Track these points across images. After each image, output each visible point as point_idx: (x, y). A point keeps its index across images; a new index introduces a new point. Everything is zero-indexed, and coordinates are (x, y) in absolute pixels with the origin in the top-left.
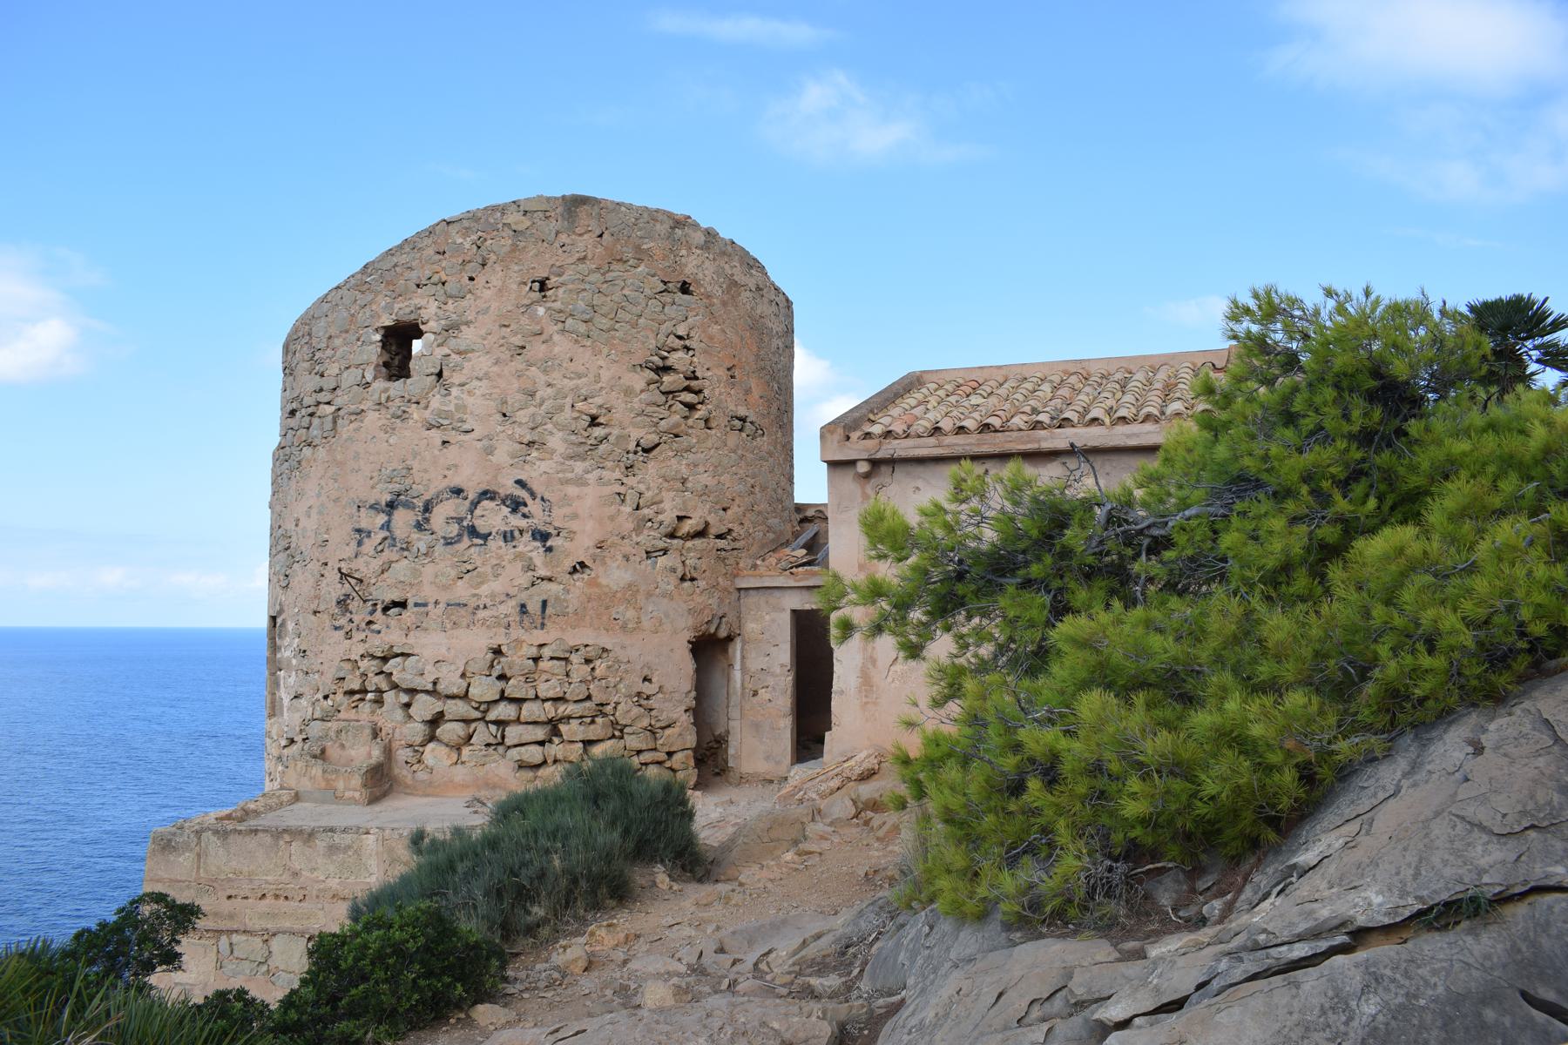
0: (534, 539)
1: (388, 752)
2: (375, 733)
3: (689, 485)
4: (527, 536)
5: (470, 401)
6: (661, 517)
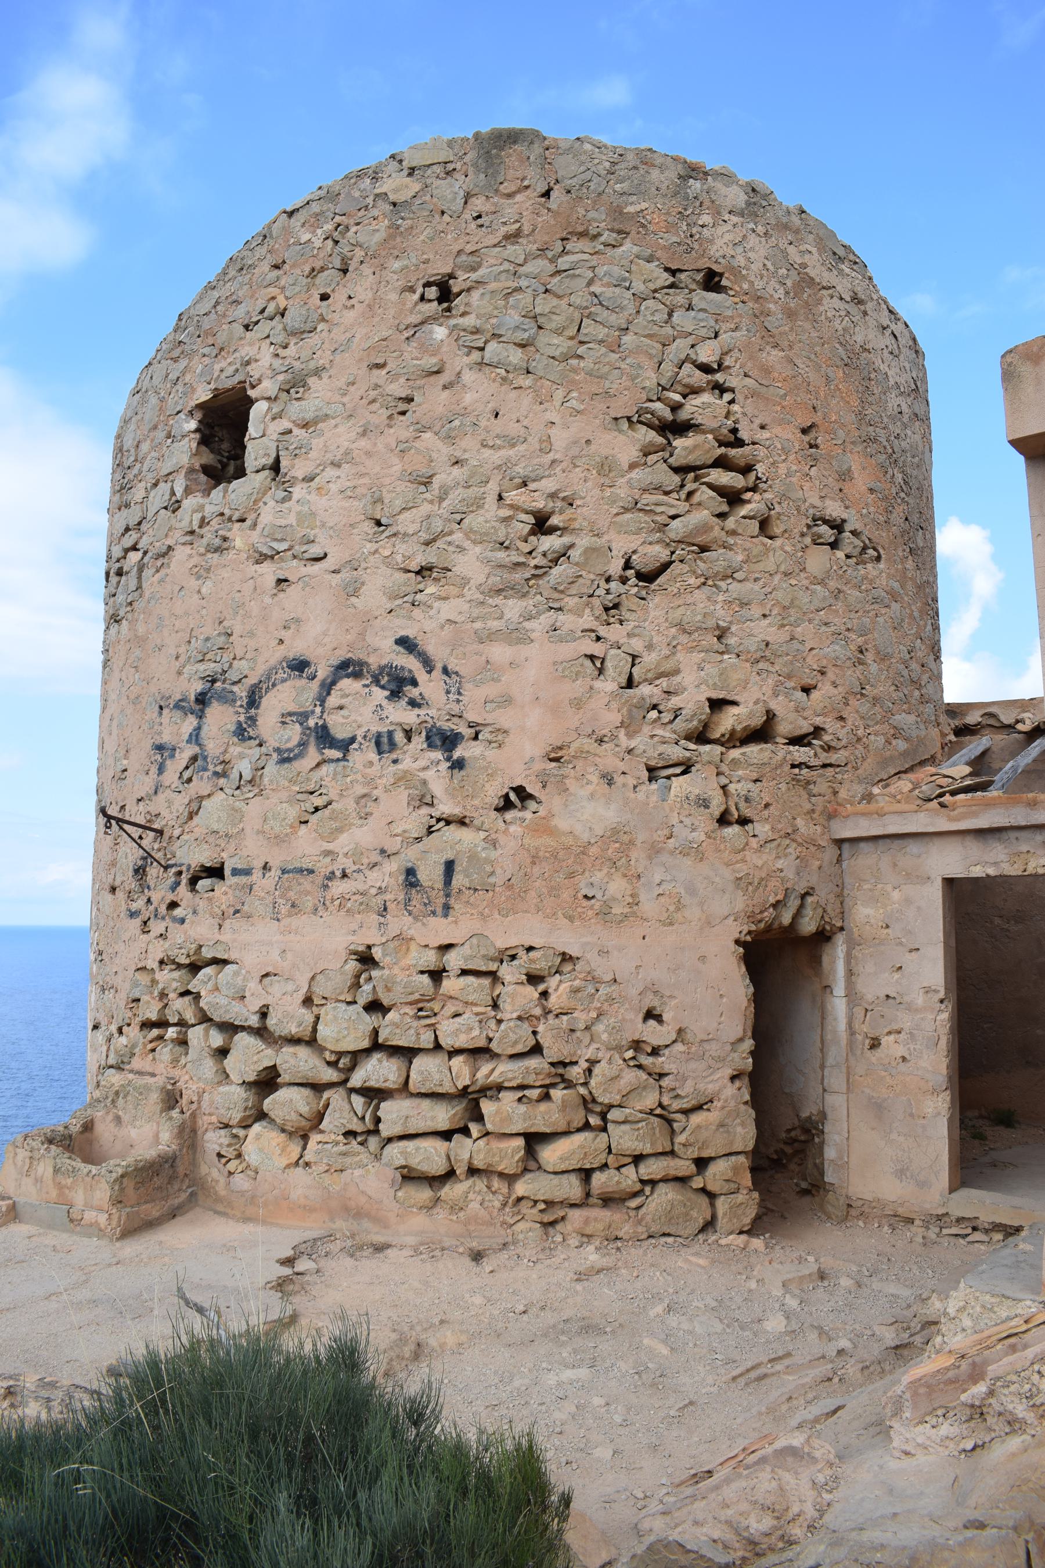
0: (431, 746)
1: (189, 1135)
2: (171, 1099)
3: (732, 641)
4: (419, 741)
5: (320, 503)
6: (675, 701)
